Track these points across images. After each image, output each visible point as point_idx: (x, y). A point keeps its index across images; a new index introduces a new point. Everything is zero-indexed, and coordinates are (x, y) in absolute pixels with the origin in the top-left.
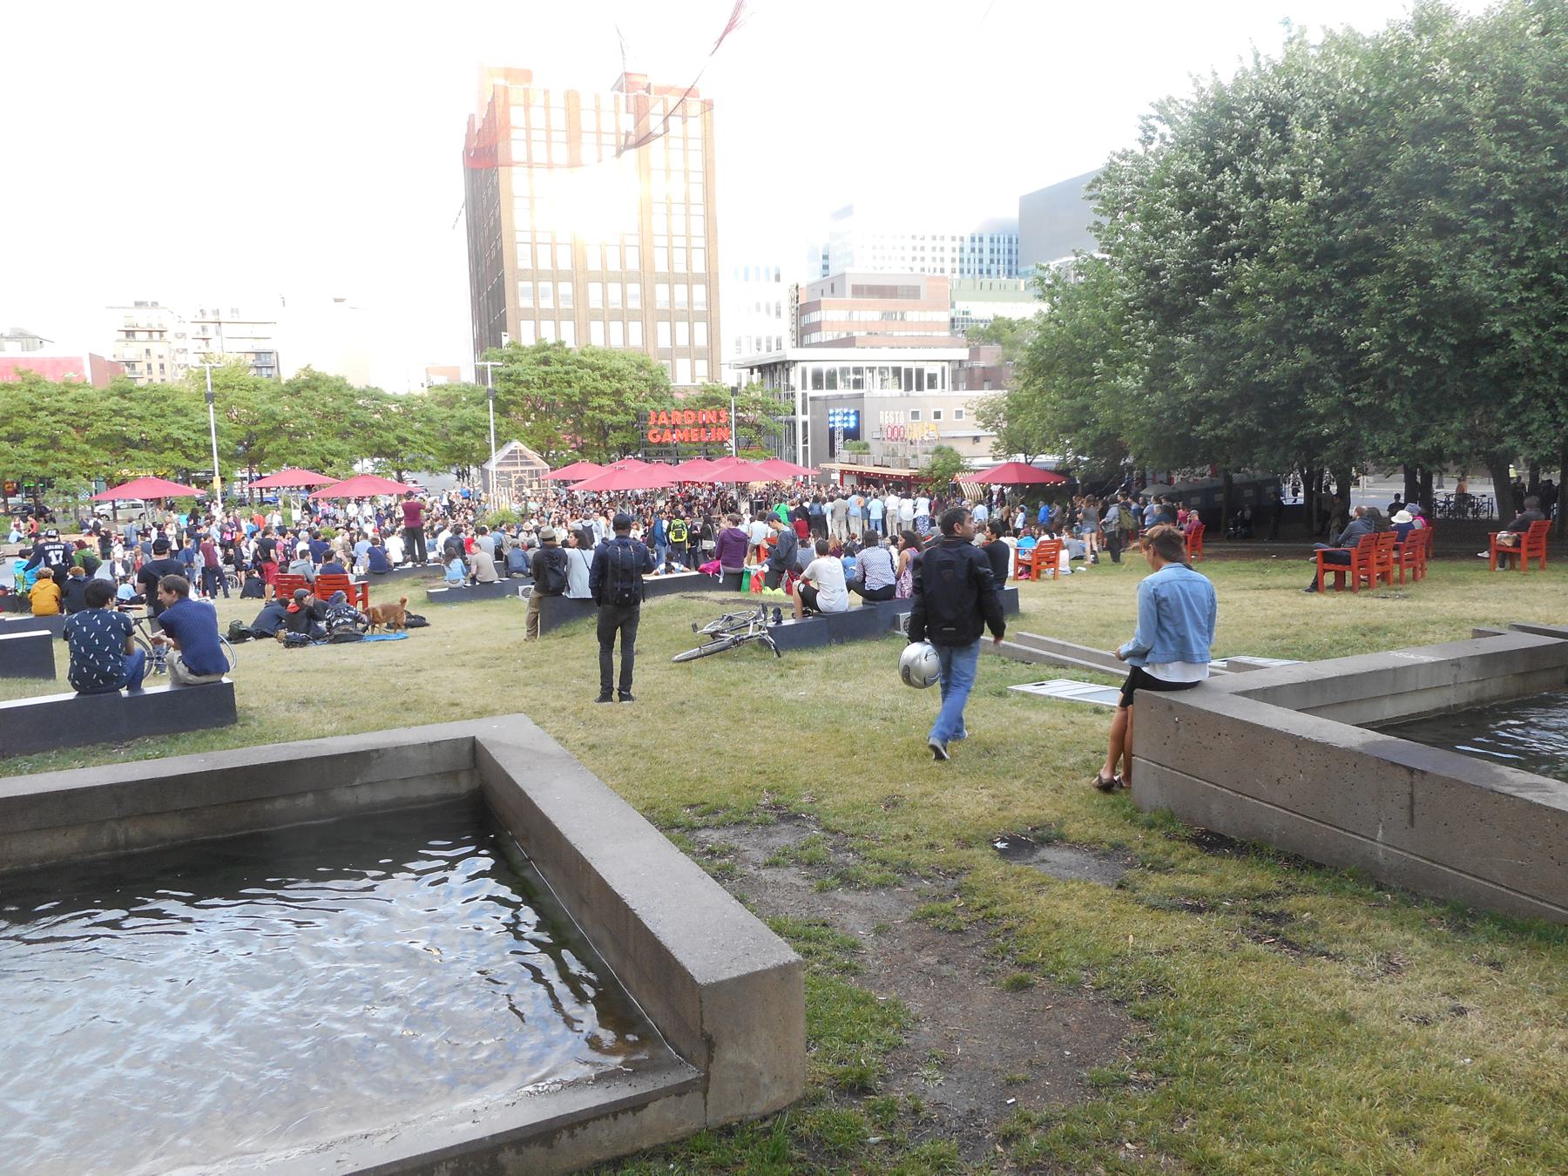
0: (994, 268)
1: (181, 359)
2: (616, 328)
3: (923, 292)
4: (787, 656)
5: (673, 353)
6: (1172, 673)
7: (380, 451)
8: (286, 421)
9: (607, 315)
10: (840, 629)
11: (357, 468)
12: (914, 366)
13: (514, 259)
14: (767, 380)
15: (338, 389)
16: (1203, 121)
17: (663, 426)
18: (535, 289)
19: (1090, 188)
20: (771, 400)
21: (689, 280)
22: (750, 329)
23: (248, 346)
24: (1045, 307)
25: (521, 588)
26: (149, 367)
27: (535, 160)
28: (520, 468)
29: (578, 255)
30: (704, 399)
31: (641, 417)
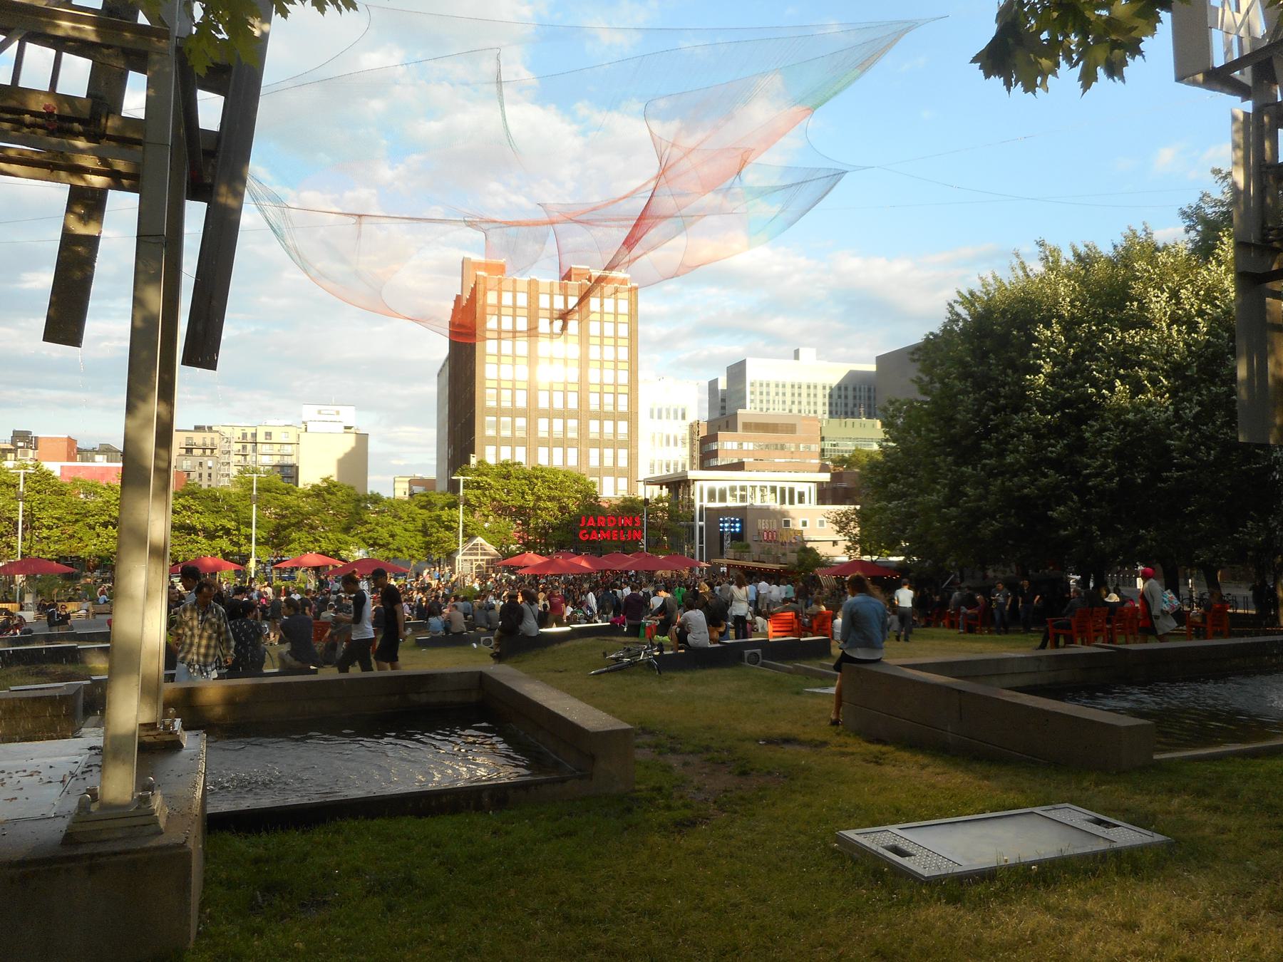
2: (558, 452)
3: (798, 428)
5: (601, 471)
6: (860, 654)
9: (550, 443)
12: (787, 486)
13: (484, 401)
18: (498, 422)
21: (615, 417)
23: (276, 460)
26: (200, 475)
27: (518, 353)
28: (479, 557)
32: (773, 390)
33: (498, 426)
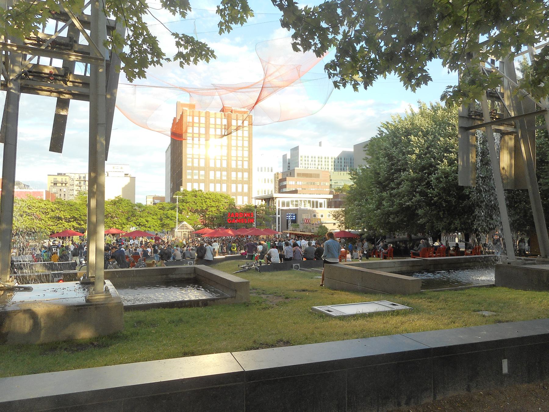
1: (71, 193)
2: (218, 185)
4: (262, 273)
5: (236, 194)
10: (275, 267)
12: (315, 200)
16: (412, 124)
18: (192, 173)
19: (365, 147)
21: (243, 171)
24: (351, 183)
26: (60, 195)
29: (207, 161)
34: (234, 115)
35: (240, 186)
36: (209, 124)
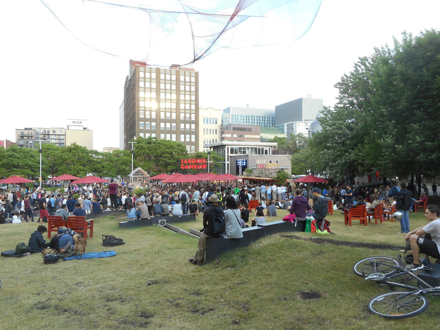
0: (268, 125)
7: (95, 171)
8: (66, 159)
9: (166, 132)
11: (88, 175)
12: (261, 147)
14: (216, 151)
15: (84, 151)
17: (185, 164)
18: (145, 124)
20: (218, 156)
22: (206, 139)
25: (160, 221)
28: (140, 176)
30: (197, 156)
31: (178, 161)
32: (239, 118)
33: (145, 125)
34: (182, 72)
35: (188, 136)
36: (180, 81)
